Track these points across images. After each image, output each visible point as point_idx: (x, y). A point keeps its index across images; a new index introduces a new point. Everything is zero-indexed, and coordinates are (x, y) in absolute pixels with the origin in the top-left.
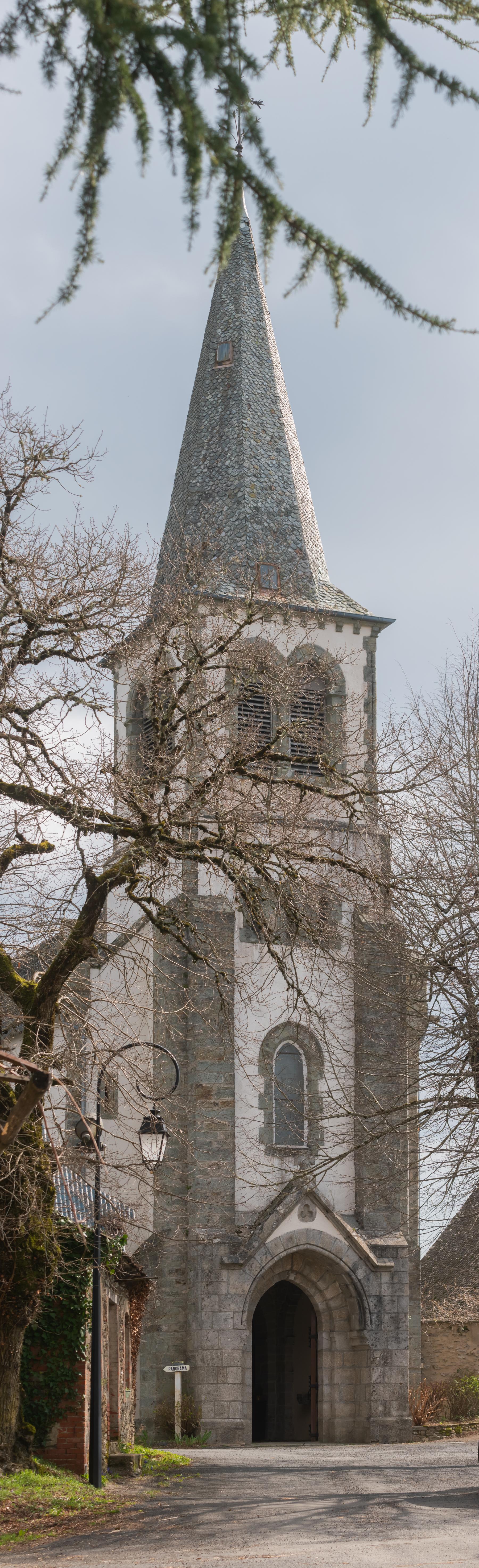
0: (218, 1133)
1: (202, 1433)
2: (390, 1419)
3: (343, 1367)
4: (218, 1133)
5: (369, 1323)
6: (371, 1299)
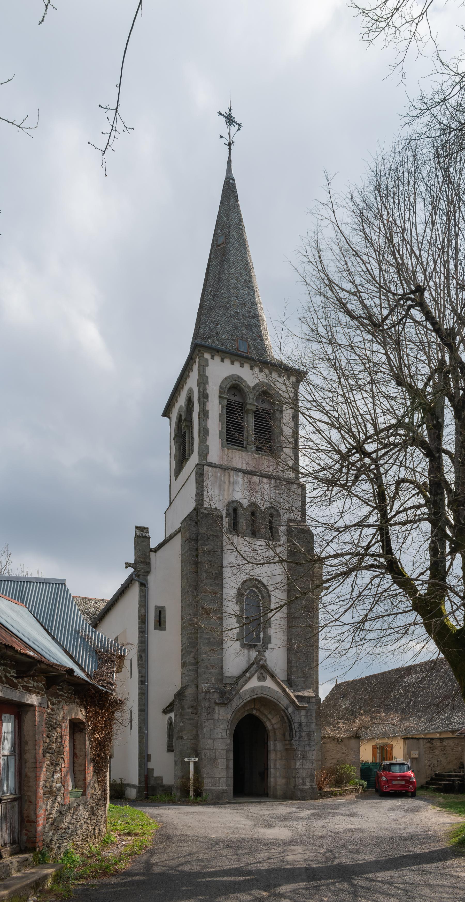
1: (204, 795)
2: (306, 787)
3: (281, 759)
6: (296, 724)
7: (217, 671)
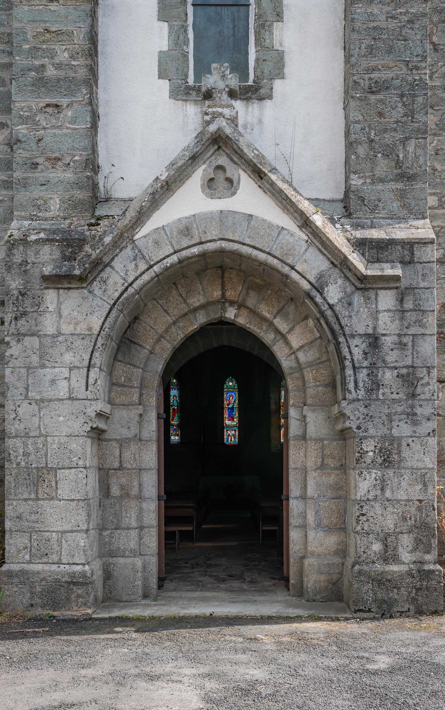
0: (57, 48)
2: (395, 568)
3: (322, 467)
4: (57, 48)
5: (351, 386)
7: (69, 175)
